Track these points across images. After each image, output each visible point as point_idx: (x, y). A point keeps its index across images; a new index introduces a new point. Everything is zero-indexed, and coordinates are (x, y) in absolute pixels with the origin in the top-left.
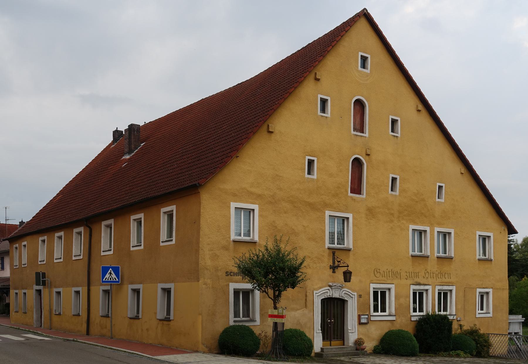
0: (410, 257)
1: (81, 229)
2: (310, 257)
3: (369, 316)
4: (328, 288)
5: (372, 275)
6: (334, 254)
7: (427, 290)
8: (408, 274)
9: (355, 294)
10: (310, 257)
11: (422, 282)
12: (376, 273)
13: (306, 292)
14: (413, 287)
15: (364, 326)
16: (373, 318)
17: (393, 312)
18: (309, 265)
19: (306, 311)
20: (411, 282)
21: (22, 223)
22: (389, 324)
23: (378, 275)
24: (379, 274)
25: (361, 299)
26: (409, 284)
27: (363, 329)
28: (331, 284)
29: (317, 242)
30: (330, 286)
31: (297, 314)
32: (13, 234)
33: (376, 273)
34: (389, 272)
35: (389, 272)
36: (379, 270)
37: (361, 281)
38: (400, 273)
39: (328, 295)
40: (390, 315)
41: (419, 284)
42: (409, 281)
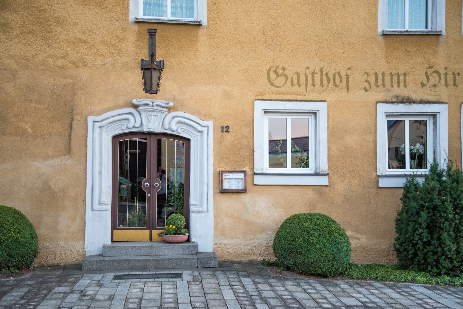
0: (381, 39)
1: (224, 175)
2: (85, 43)
3: (250, 175)
4: (131, 110)
5: (263, 80)
6: (152, 34)
7: (434, 116)
8: (372, 79)
9: (211, 124)
10: (85, 43)
11: (415, 96)
12: (273, 76)
13: (72, 119)
14: (383, 109)
15: (236, 196)
16: (259, 180)
17: (324, 166)
18: (82, 60)
19: (67, 161)
20: (382, 96)
21: (396, 225)
22: (311, 193)
23: (280, 81)
24: (283, 79)
25: (229, 137)
26: (374, 100)
27: (228, 202)
28: (135, 101)
29: (105, 8)
30: (136, 107)
31: (44, 167)
32: (198, 191)
33: (273, 76)
34: (313, 74)
35: (313, 74)
36: (284, 69)
37: (227, 95)
38: (347, 77)
39: (131, 125)
40: (316, 174)
41: (408, 101)
42: (373, 96)
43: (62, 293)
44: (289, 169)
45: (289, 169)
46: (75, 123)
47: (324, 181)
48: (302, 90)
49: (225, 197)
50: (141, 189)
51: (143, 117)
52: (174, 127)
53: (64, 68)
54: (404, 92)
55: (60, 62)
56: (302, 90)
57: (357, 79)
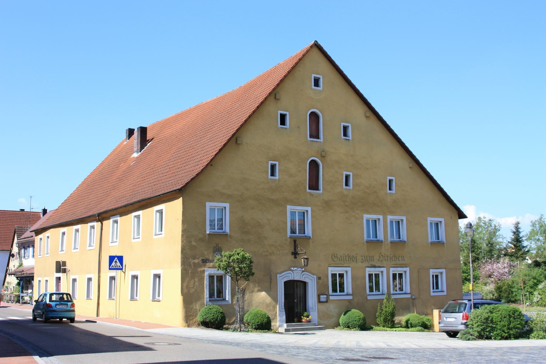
8: (363, 258)
9: (315, 277)
11: (377, 265)
12: (333, 257)
13: (271, 276)
20: (367, 264)
23: (335, 259)
25: (320, 281)
27: (323, 307)
33: (333, 257)
41: (374, 267)
42: (365, 265)
43: (284, 348)
44: (338, 293)
45: (398, 292)
46: (272, 277)
47: (350, 297)
48: (343, 262)
49: (320, 304)
50: (490, 300)
51: (295, 274)
52: (302, 279)
53: (266, 256)
54: (374, 263)
55: (266, 253)
56: (343, 262)
57: (359, 258)
